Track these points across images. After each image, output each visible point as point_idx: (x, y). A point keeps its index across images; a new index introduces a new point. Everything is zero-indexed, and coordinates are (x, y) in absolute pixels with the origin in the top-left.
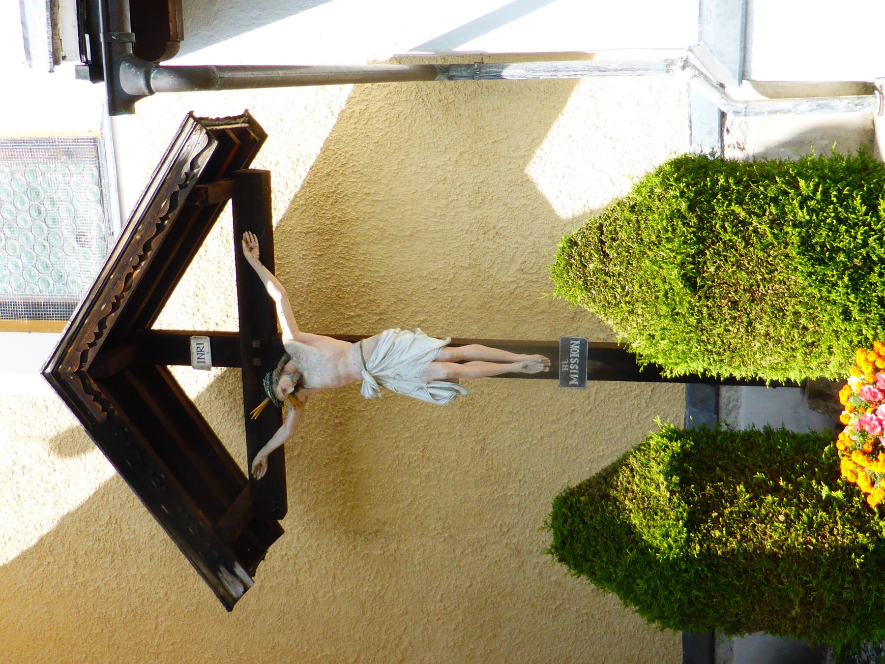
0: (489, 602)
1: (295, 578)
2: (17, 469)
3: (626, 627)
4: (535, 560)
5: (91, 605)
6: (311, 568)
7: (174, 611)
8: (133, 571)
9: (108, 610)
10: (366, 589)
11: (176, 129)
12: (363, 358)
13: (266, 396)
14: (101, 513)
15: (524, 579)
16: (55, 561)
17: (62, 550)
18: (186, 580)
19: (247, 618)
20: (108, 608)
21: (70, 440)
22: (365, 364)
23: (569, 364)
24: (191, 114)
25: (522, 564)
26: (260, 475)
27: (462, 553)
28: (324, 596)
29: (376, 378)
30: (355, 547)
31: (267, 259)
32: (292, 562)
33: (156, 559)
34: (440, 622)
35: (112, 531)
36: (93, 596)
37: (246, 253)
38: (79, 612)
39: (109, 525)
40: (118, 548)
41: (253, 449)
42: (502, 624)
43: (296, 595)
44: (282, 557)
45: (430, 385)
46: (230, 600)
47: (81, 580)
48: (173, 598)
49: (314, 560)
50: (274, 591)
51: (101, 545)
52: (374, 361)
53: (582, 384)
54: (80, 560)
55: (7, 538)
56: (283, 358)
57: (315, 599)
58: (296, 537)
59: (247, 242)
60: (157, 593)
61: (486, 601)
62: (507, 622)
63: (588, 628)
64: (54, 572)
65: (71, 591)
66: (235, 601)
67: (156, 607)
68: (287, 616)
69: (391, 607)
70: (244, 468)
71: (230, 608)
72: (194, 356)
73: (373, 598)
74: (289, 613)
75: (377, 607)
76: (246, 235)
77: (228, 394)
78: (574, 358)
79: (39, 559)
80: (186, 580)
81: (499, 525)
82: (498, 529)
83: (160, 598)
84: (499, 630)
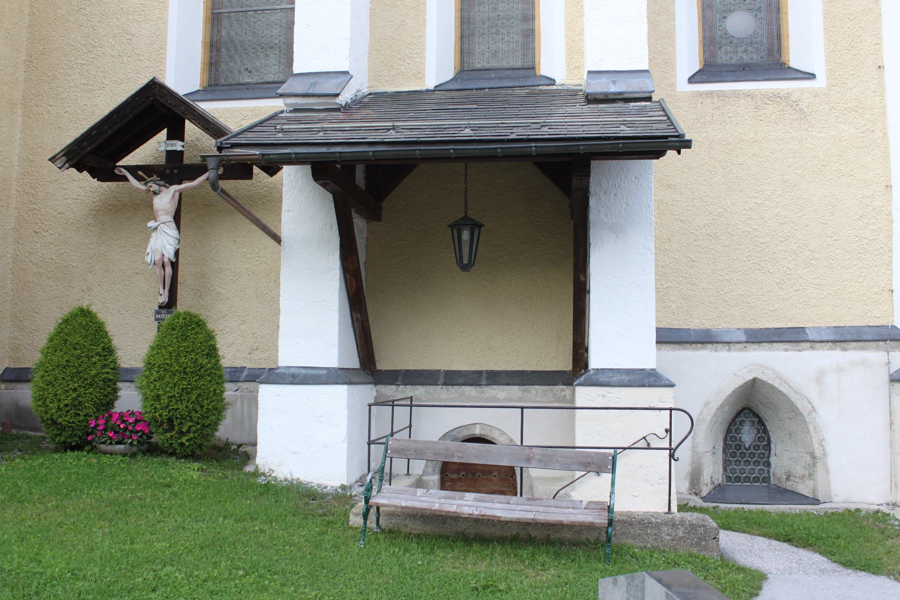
2: (130, 37)
8: (79, 95)
13: (149, 178)
21: (144, 66)
26: (116, 171)
30: (91, 210)
32: (84, 178)
33: (85, 107)
40: (90, 87)
41: (127, 168)
46: (54, 160)
48: (66, 115)
54: (84, 67)
55: (95, 28)
56: (167, 185)
66: (53, 163)
70: (120, 163)
71: (50, 160)
72: (170, 142)
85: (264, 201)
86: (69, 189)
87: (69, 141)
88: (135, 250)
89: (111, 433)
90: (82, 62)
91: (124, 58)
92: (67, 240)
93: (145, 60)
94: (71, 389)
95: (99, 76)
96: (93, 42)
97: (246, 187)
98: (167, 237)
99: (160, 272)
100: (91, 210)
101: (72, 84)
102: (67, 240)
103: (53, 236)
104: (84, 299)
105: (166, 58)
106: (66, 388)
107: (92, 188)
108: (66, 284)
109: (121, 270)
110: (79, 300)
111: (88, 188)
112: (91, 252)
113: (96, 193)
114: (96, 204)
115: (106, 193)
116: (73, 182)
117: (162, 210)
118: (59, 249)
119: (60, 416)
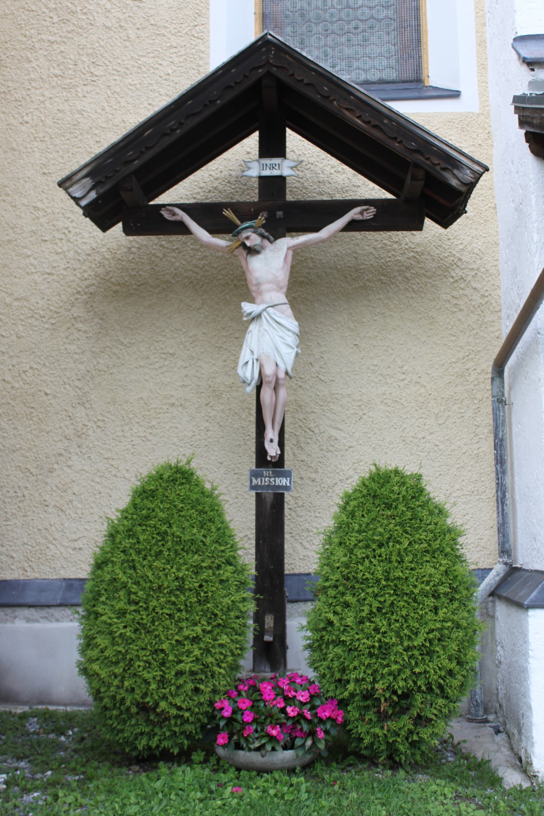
0: (32, 410)
1: (46, 239)
3: (12, 531)
4: (72, 450)
5: (13, 53)
6: (57, 254)
7: (11, 129)
8: (47, 93)
9: (8, 69)
10: (40, 302)
11: (476, 157)
12: (277, 305)
13: (242, 222)
14: (101, 68)
15: (54, 441)
16: (54, 24)
17: (64, 30)
18: (41, 141)
19: (8, 195)
20: (11, 69)
21: (168, 45)
22: (272, 306)
23: (270, 477)
24: (487, 170)
25: (68, 439)
26: (165, 214)
27: (77, 387)
28: (32, 264)
29: (259, 316)
30: (79, 293)
31: (351, 226)
33: (60, 115)
34: (11, 367)
35: (84, 76)
36: (22, 56)
37: (358, 209)
38: (6, 42)
39: (90, 75)
40: (68, 81)
42: (11, 422)
43: (31, 239)
44: (67, 228)
45: (255, 361)
46: (67, 184)
47: (37, 46)
48: (23, 128)
49: (65, 256)
50: (34, 219)
51: (71, 66)
52: (275, 314)
53: (252, 488)
54: (55, 47)
56: (271, 237)
57: (29, 256)
58: (86, 241)
59: (367, 209)
60: (27, 114)
61: (33, 408)
62: (12, 426)
63: (10, 497)
64: (43, 22)
65: (25, 36)
67: (13, 112)
68: (11, 231)
69: (23, 323)
71: (61, 184)
73: (32, 308)
74: (14, 232)
75: (23, 312)
76: (373, 210)
77: (215, 186)
78: (275, 481)
79: (56, 9)
80: (41, 141)
81: (104, 418)
82: (100, 418)
83: (23, 117)
84: (6, 419)
85: (408, 275)
86: (35, 255)
87: (98, 149)
88: (167, 363)
89: (273, 728)
90: (50, 38)
91: (130, 32)
92: (33, 346)
93: (169, 36)
94: (187, 638)
95: (83, 62)
96: (70, 5)
97: (373, 251)
98: (282, 332)
99: (272, 396)
100: (79, 293)
101: (33, 76)
102: (33, 346)
103: (6, 340)
104: (70, 453)
105: (208, 31)
106: (177, 637)
107: (79, 254)
108: (33, 427)
109: (141, 398)
110: (60, 455)
111: (71, 254)
112: (81, 367)
113: (87, 263)
114: (87, 283)
115: (106, 262)
116: (43, 244)
117: (270, 282)
118: (19, 363)
119: (164, 697)
